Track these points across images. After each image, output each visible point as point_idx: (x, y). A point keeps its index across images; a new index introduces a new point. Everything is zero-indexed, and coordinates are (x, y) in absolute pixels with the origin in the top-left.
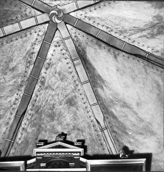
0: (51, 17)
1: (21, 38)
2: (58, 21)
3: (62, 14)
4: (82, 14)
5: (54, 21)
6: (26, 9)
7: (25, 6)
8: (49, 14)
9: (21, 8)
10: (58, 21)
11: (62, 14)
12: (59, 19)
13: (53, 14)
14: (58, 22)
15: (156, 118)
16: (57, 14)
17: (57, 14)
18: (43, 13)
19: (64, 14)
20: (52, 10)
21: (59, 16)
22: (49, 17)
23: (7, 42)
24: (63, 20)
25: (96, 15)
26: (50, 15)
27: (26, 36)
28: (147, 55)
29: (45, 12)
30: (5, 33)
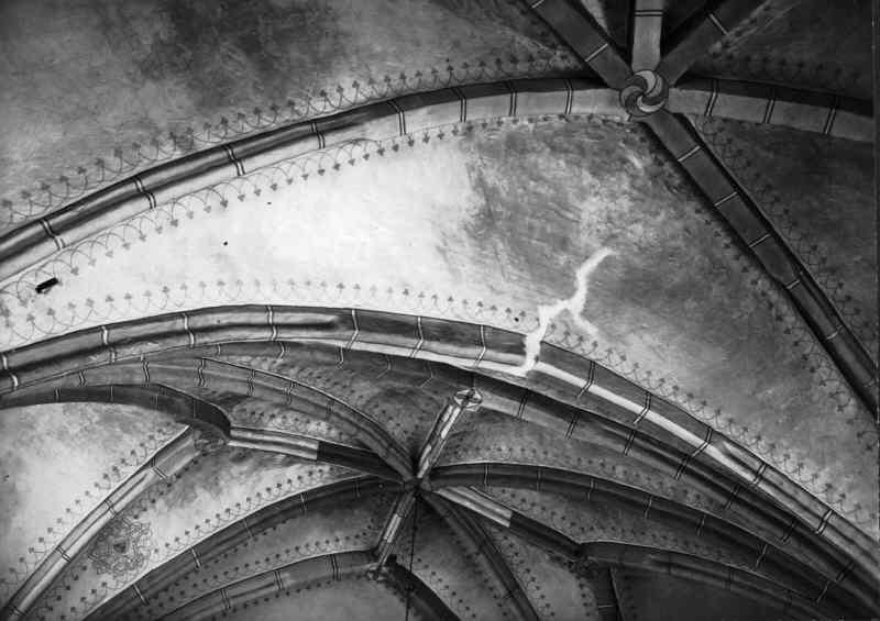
0: (664, 95)
1: (783, 63)
2: (650, 77)
3: (626, 93)
4: (559, 59)
5: (660, 81)
6: (715, 134)
7: (714, 145)
8: (663, 108)
9: (730, 141)
10: (650, 77)
11: (626, 93)
12: (643, 83)
13: (653, 102)
14: (649, 73)
15: (852, 273)
16: (640, 99)
17: (640, 99)
18: (681, 118)
19: (621, 91)
20: (648, 114)
21: (638, 89)
22: (667, 97)
23: (838, 71)
24: (633, 73)
25: (517, 39)
26: (660, 105)
27: (765, 60)
28: (259, 382)
29: (671, 117)
30: (830, 115)
